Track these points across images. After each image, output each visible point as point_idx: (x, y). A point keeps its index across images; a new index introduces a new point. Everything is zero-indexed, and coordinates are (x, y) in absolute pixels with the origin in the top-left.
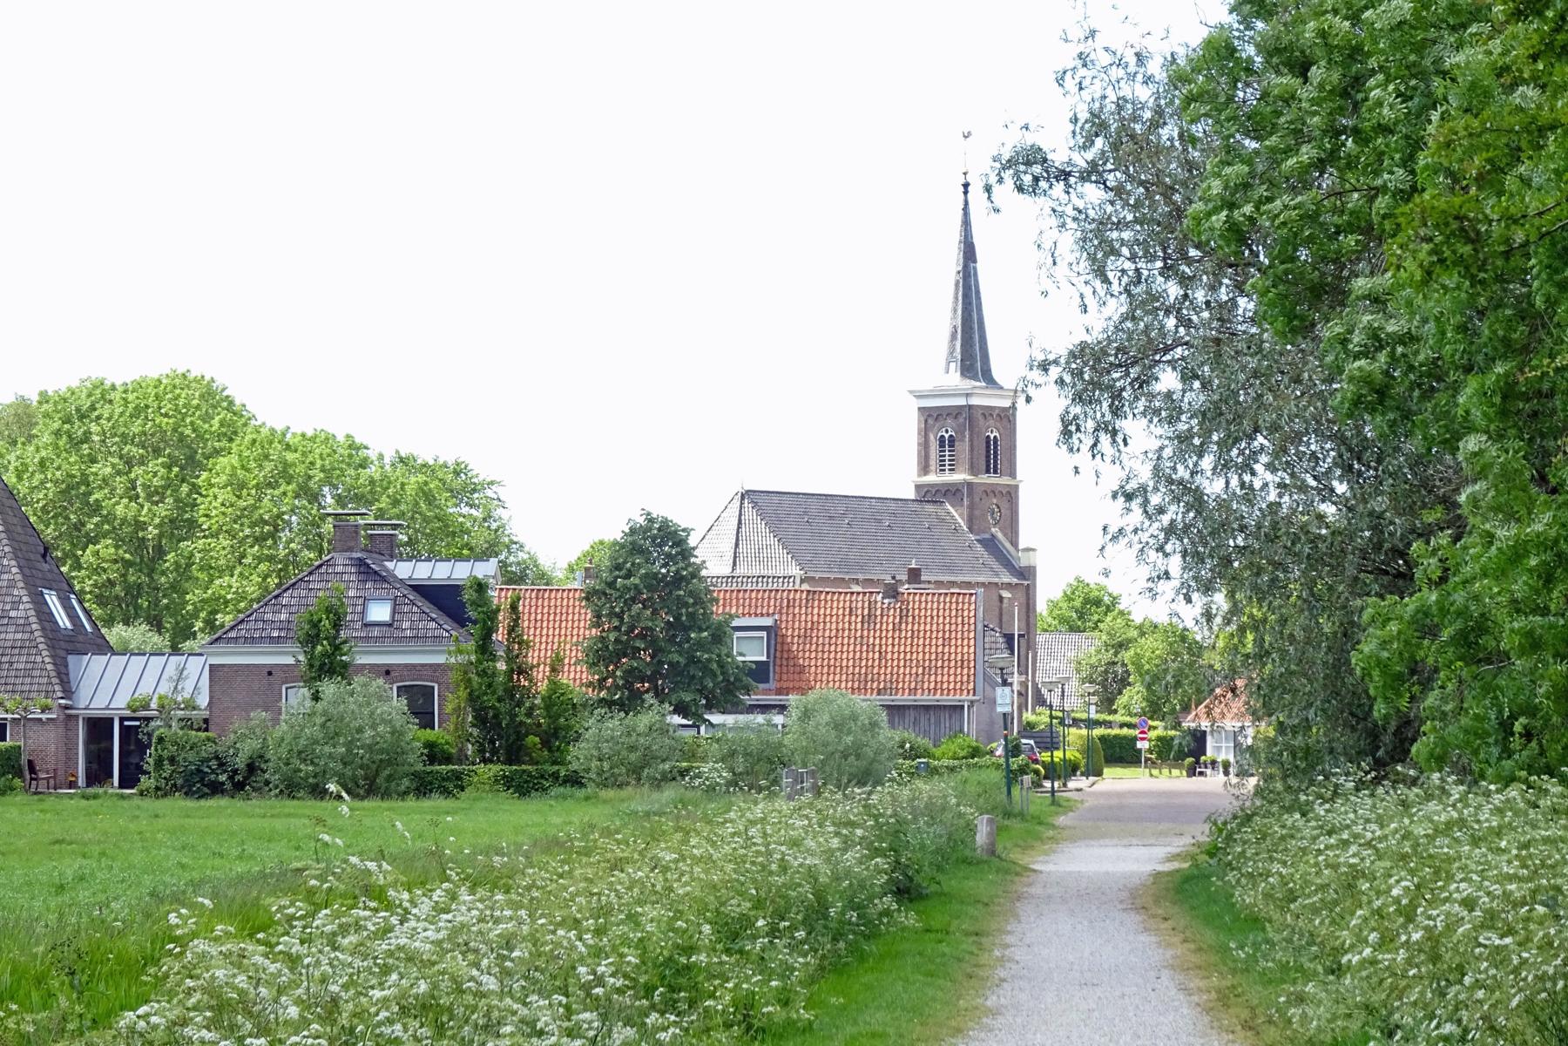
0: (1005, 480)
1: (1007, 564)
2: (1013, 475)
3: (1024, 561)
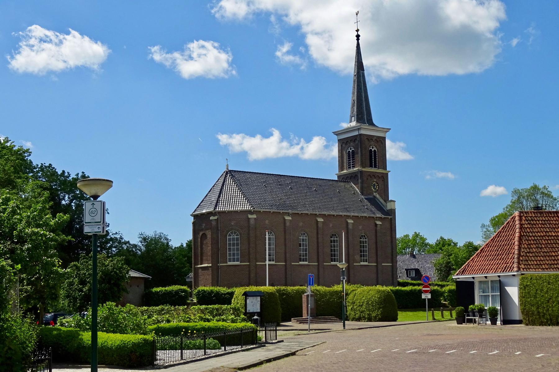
0: (381, 171)
1: (380, 208)
2: (385, 168)
3: (389, 206)
